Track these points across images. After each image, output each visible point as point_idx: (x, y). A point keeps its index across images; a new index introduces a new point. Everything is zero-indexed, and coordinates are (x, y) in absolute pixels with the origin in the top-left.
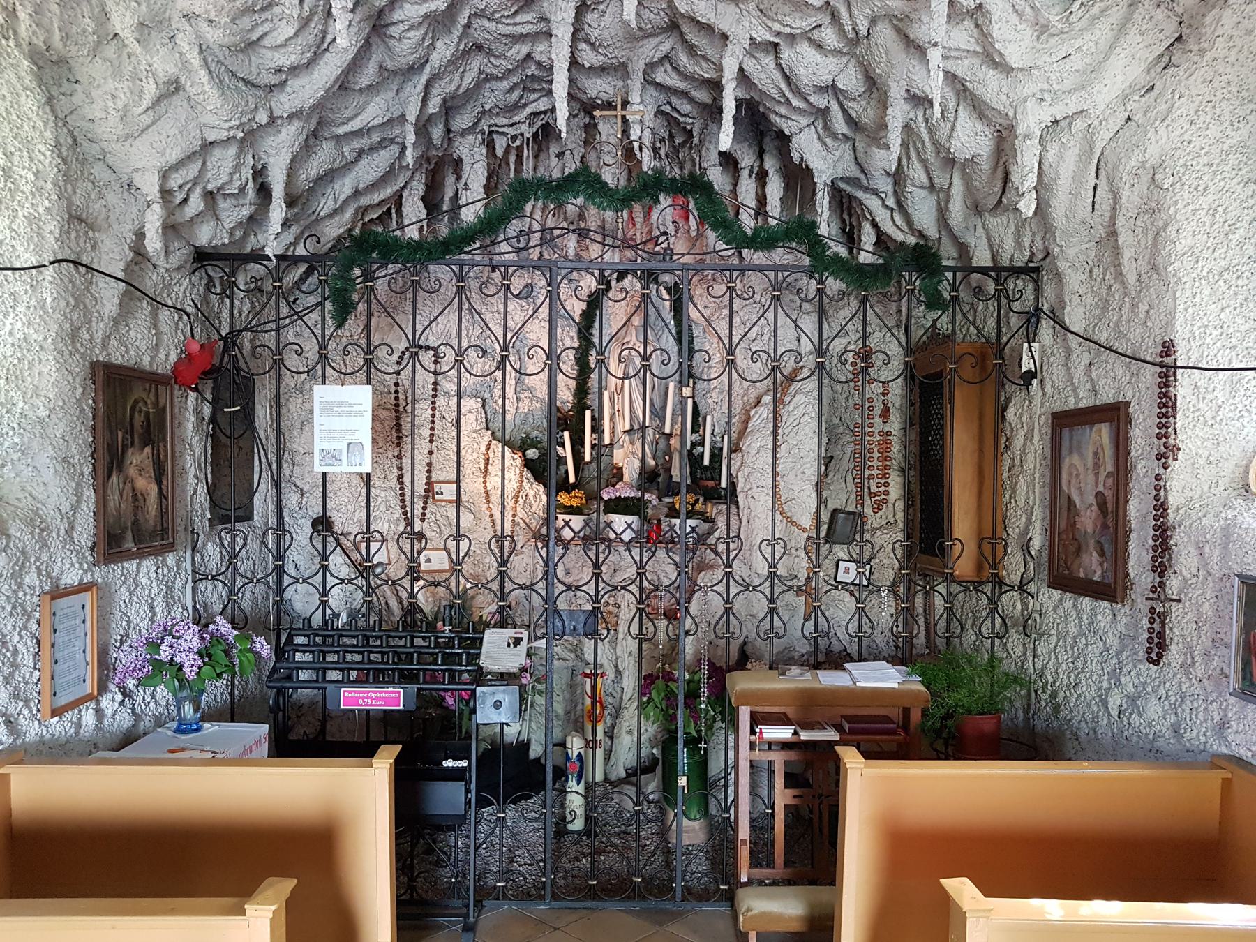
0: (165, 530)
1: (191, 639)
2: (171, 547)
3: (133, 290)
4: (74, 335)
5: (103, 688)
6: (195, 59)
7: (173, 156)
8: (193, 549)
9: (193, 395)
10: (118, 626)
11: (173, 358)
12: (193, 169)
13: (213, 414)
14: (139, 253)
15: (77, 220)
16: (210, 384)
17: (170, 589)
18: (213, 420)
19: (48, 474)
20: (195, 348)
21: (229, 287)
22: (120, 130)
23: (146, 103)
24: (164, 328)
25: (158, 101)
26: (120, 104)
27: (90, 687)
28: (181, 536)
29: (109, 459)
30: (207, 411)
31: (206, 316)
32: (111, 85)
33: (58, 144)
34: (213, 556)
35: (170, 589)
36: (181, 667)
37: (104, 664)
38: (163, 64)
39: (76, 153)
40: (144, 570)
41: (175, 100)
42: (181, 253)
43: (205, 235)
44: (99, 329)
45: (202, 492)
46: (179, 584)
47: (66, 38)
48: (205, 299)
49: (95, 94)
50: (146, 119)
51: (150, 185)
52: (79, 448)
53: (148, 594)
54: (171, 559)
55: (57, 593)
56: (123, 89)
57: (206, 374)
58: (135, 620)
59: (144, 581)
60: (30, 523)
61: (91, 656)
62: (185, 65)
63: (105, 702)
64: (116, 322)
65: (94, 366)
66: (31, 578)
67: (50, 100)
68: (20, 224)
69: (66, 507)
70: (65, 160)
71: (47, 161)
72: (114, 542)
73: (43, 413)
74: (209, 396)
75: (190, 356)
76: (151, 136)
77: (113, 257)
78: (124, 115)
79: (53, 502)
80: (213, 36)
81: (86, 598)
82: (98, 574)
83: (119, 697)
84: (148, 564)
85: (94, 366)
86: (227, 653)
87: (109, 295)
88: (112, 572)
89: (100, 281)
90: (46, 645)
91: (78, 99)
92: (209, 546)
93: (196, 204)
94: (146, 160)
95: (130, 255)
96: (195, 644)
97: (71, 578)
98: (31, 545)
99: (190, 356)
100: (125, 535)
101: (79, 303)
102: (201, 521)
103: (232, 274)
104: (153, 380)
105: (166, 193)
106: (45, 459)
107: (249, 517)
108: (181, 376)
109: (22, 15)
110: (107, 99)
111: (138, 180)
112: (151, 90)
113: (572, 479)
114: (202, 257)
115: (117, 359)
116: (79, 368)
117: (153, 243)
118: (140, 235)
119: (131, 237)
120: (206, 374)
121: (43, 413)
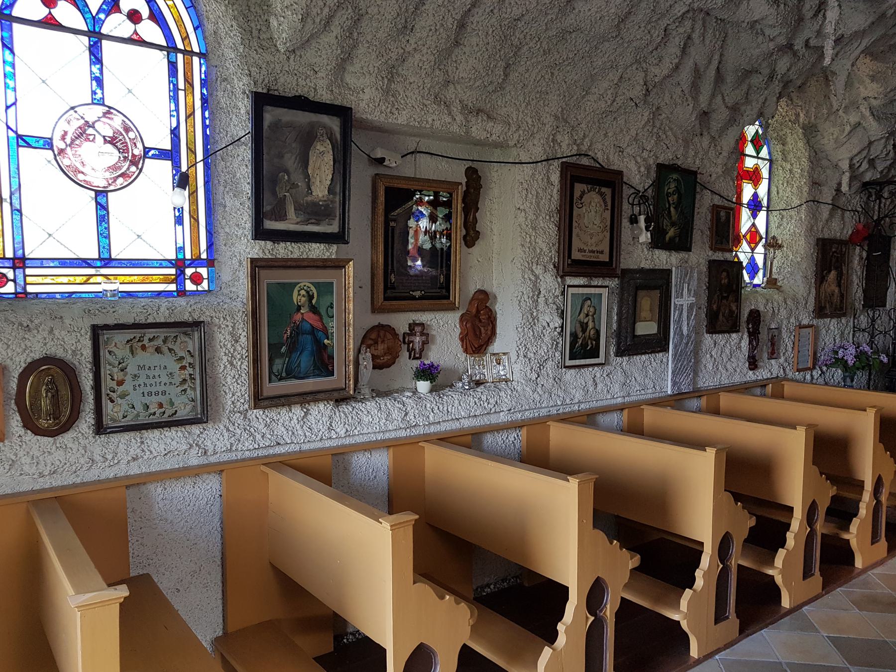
0: (841, 308)
1: (852, 350)
2: (844, 315)
3: (835, 206)
4: (811, 229)
5: (814, 368)
6: (868, 114)
7: (855, 152)
8: (854, 318)
9: (858, 248)
10: (821, 344)
11: (850, 232)
12: (865, 153)
13: (868, 256)
14: (838, 190)
15: (815, 184)
16: (867, 242)
17: (842, 333)
18: (868, 258)
19: (800, 282)
20: (861, 227)
21: (879, 197)
22: (835, 146)
23: (846, 132)
24: (847, 220)
25: (851, 131)
26: (835, 136)
27: (810, 365)
28: (849, 310)
29: (820, 278)
30: (864, 254)
31: (866, 211)
32: (832, 130)
33: (810, 156)
34: (864, 321)
35: (842, 333)
36: (846, 361)
37: (815, 359)
38: (853, 118)
39: (816, 157)
40: (832, 323)
41: (858, 129)
42: (857, 185)
43: (868, 177)
44: (820, 225)
45: (860, 291)
46: (846, 332)
47: (816, 118)
48: (866, 203)
49: (825, 134)
50: (845, 140)
51: (845, 165)
52: (811, 273)
53: (833, 331)
54: (844, 320)
55: (801, 327)
56: (836, 131)
57: (865, 239)
58: (828, 343)
59: (832, 328)
60: (793, 300)
61: (811, 353)
62: (863, 116)
63: (814, 373)
64: (827, 221)
65: (818, 240)
66: (792, 320)
67: (808, 142)
68: (795, 190)
69: (805, 295)
70: (812, 162)
71: (805, 163)
72: (820, 312)
73: (799, 259)
74: (866, 248)
75: (858, 231)
76: (847, 145)
77: (827, 195)
78: (836, 141)
79: (800, 293)
80: (875, 103)
81: (810, 330)
82: (815, 322)
83: (820, 372)
84: (834, 321)
85: (818, 240)
86: (867, 359)
87: (825, 211)
88: (820, 322)
89: (822, 206)
90: (796, 345)
91: (819, 137)
92: (862, 317)
93: (865, 165)
94: (843, 157)
95: (834, 193)
96: (854, 351)
97: (805, 322)
98: (794, 308)
99: (858, 231)
100: (828, 307)
101: (814, 215)
102: (859, 305)
103: (881, 190)
104: (841, 242)
105: (851, 166)
106: (799, 277)
107: (885, 306)
108: (855, 239)
109: (801, 115)
110: (829, 135)
111: (840, 164)
112: (848, 128)
113: (204, 256)
114: (866, 185)
115: (826, 236)
116: (813, 241)
117: (845, 188)
118: (840, 184)
119: (835, 186)
120: (865, 239)
121: (799, 259)
